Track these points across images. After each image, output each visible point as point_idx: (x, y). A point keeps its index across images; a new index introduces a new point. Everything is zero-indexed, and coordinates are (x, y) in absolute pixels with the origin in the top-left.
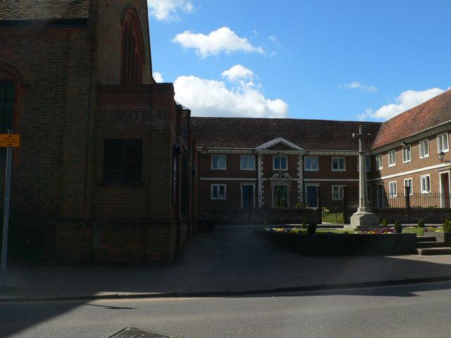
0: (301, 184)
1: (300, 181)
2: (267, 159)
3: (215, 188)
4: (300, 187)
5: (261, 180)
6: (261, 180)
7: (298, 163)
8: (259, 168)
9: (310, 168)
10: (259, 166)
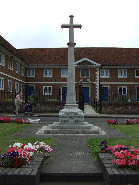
1: (97, 83)
3: (120, 89)
9: (104, 76)
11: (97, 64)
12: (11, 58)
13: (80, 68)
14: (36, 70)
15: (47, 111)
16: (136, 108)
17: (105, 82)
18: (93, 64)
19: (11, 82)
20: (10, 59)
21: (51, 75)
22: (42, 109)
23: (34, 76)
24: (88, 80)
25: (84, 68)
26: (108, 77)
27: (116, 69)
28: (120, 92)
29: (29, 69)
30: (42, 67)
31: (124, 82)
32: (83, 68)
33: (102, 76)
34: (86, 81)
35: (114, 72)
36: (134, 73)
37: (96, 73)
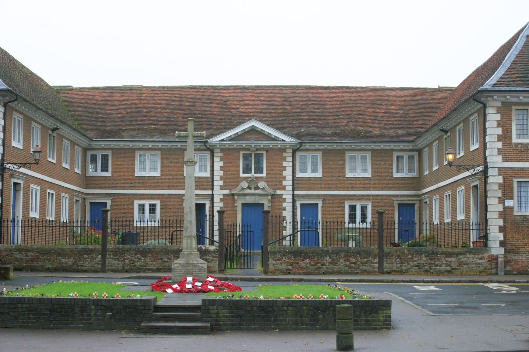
0: (289, 200)
1: (287, 194)
2: (229, 153)
3: (353, 208)
4: (288, 204)
5: (219, 192)
6: (219, 192)
7: (285, 164)
8: (215, 173)
9: (306, 171)
10: (217, 168)
11: (287, 139)
12: (53, 130)
13: (238, 150)
14: (113, 156)
15: (150, 269)
16: (341, 260)
17: (310, 190)
18: (275, 139)
19: (53, 194)
20: (50, 135)
21: (155, 170)
22: (138, 264)
23: (107, 171)
24: (261, 184)
25: (249, 149)
26: (319, 174)
27: (342, 152)
28: (353, 219)
29: (94, 153)
30: (131, 145)
31: (364, 189)
32: (245, 149)
33: (301, 171)
34: (257, 188)
35: (334, 158)
36: (392, 166)
37: (285, 164)
